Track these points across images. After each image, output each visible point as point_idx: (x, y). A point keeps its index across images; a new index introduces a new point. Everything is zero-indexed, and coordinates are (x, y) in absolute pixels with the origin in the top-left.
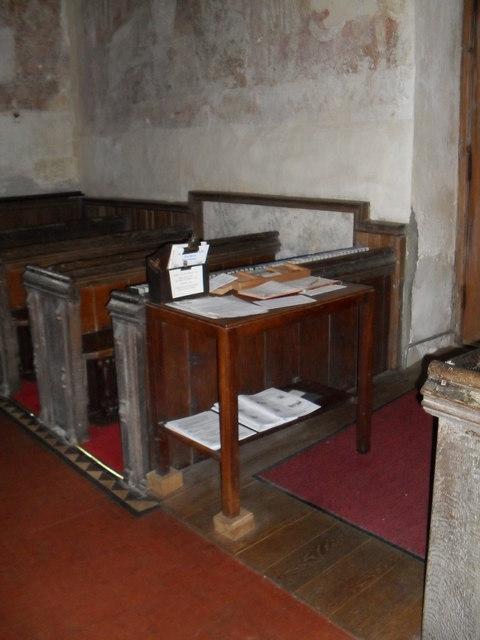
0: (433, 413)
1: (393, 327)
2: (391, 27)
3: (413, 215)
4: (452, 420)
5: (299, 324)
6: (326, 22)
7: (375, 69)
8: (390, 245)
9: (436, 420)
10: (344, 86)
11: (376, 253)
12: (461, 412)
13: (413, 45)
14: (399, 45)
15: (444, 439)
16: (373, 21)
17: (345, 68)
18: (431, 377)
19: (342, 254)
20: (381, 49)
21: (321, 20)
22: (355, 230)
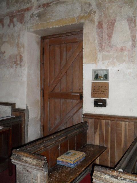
0: (15, 164)
1: (23, 138)
2: (21, 57)
3: (27, 107)
4: (19, 165)
5: (3, 135)
6: (5, 54)
7: (17, 67)
8: (21, 115)
9: (16, 165)
10: (9, 72)
11: (17, 117)
12: (21, 163)
13: (26, 62)
14: (23, 62)
15: (18, 171)
16: (16, 55)
17: (9, 67)
18: (13, 154)
19: (6, 118)
20: (18, 62)
21: (3, 54)
22: (12, 111)
